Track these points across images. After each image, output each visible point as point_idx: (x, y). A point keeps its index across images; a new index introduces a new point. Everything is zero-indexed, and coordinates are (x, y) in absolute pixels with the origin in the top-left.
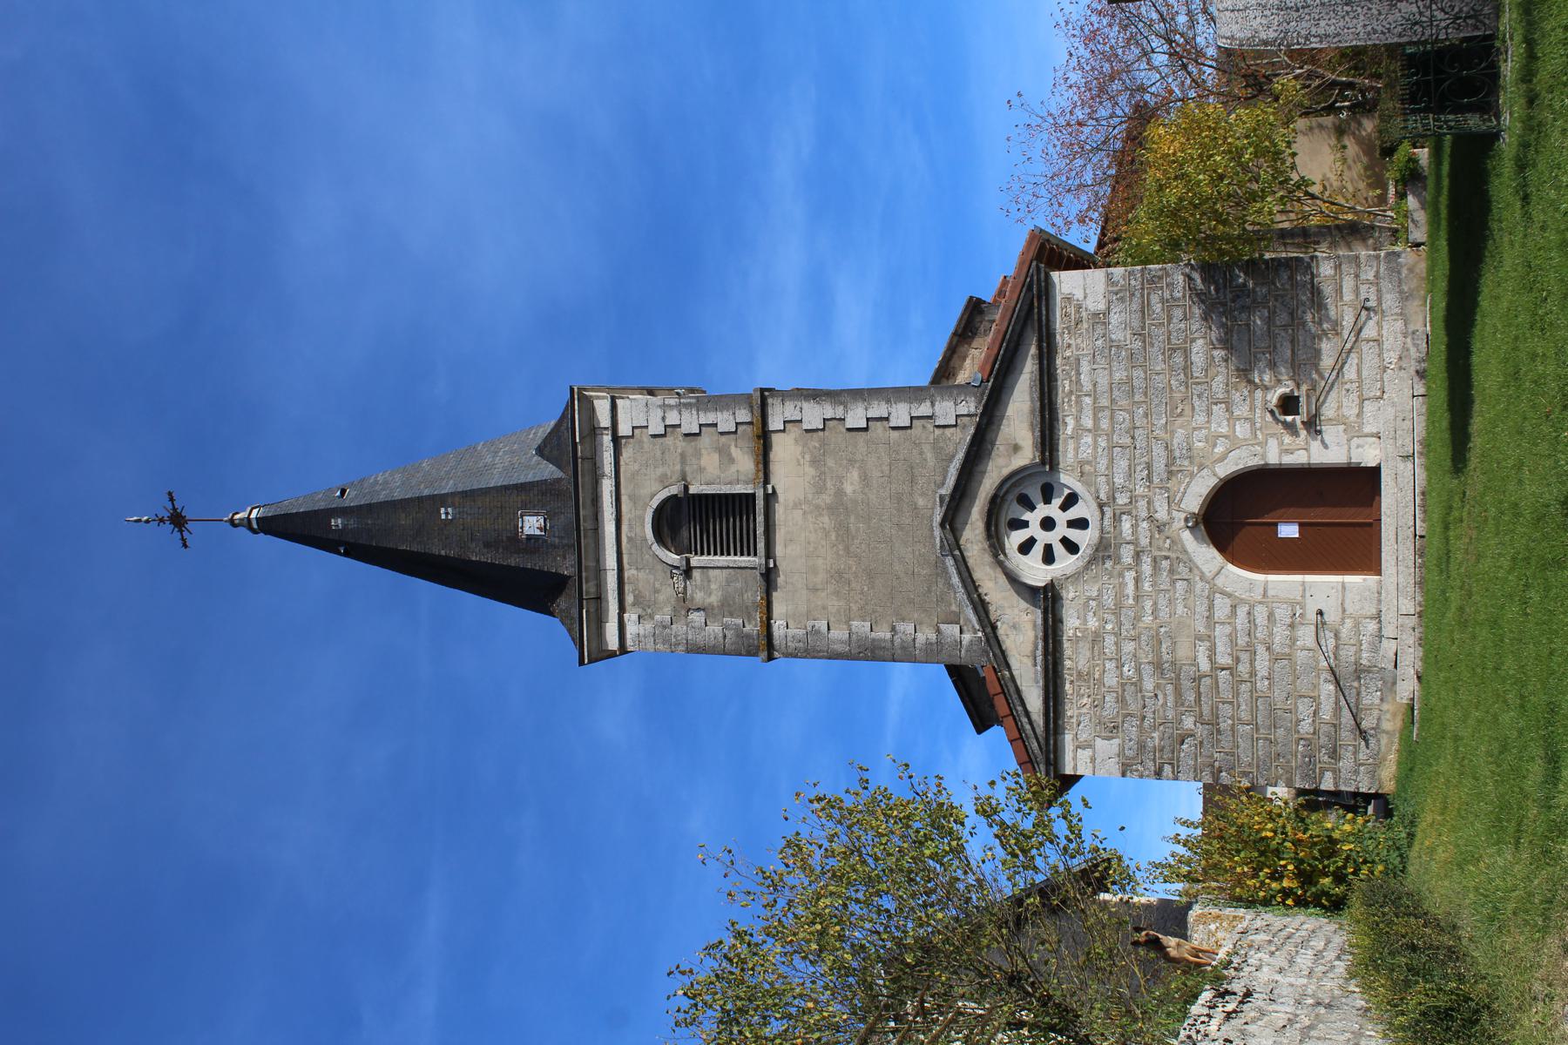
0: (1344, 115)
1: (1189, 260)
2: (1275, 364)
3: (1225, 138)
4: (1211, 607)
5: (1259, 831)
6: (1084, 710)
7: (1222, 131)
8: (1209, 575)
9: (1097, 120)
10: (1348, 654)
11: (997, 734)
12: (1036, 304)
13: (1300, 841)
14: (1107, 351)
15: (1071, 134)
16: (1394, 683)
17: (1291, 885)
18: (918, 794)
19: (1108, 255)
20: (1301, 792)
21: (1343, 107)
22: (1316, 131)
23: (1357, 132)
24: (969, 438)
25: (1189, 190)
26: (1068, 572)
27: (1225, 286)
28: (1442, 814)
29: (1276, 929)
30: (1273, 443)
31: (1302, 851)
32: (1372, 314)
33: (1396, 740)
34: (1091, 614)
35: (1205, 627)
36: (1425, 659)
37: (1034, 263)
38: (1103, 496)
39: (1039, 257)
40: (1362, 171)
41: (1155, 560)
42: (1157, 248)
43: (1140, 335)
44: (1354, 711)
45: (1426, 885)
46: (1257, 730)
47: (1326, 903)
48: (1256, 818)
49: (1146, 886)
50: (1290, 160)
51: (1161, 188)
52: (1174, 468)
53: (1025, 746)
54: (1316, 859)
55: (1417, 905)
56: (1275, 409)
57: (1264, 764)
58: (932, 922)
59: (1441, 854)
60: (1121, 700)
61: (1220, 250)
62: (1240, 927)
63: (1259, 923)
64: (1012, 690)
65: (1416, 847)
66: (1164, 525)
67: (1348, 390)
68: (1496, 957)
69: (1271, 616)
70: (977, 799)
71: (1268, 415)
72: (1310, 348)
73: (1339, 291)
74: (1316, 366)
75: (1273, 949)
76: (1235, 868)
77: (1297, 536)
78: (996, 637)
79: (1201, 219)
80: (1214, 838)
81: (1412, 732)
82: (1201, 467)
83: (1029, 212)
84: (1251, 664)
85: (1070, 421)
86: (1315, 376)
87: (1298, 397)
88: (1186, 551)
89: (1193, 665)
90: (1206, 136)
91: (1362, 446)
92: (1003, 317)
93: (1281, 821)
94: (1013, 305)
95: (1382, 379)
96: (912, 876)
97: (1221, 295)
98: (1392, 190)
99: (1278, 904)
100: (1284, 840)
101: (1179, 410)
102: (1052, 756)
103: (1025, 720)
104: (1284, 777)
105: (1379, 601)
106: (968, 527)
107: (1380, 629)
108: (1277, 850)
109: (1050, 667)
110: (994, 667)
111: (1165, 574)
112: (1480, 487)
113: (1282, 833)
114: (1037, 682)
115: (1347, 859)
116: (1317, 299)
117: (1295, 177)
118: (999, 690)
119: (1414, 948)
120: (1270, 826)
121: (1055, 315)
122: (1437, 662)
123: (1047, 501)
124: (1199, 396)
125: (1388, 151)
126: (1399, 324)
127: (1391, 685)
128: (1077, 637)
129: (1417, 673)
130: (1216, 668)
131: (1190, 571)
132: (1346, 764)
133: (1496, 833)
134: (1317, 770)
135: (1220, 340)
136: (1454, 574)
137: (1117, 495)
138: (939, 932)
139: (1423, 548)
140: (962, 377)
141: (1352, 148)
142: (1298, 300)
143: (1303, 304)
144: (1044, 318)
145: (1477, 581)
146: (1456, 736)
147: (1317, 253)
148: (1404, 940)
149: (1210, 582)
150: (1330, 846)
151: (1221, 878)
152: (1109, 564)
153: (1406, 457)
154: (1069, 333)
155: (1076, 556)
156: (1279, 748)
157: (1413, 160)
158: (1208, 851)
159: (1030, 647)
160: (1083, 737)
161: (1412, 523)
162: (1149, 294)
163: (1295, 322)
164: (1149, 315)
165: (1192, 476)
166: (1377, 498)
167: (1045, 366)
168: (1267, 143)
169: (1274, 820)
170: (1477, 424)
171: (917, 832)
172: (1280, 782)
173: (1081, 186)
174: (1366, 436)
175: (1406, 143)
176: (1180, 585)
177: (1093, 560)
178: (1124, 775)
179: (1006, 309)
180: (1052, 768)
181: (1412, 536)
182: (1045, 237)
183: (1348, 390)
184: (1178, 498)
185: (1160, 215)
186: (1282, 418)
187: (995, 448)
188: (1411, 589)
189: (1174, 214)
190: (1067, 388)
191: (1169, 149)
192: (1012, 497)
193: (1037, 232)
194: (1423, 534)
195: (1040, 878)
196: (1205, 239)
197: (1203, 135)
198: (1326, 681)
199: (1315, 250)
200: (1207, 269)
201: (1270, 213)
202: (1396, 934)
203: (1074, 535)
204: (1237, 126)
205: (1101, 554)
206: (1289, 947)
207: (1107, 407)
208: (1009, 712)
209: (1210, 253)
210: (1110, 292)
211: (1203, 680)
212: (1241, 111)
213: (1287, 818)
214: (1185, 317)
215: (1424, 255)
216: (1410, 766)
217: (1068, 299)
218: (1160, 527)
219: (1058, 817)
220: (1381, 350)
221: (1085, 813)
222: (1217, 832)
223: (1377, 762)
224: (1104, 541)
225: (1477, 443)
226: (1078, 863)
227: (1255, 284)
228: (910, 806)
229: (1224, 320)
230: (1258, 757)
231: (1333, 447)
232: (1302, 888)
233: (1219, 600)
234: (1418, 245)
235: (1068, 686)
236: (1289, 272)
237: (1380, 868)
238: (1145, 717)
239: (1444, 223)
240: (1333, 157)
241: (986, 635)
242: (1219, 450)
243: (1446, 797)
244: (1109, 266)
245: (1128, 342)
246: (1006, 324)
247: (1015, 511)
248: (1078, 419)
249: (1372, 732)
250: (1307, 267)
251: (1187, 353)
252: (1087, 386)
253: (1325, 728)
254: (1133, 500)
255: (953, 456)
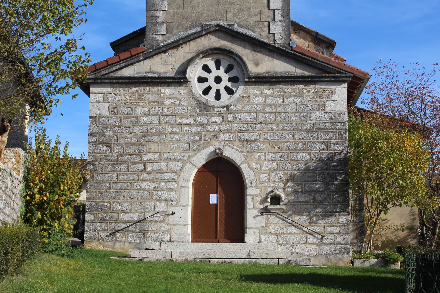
0: (419, 231)
1: (350, 153)
3: (411, 172)
4: (175, 161)
5: (63, 183)
6: (123, 97)
7: (414, 170)
8: (192, 160)
9: (424, 109)
10: (153, 227)
11: (110, 53)
12: (331, 75)
13: (59, 203)
14: (305, 111)
16: (138, 248)
17: (36, 199)
18: (77, 9)
19: (354, 112)
20: (84, 206)
21: (423, 230)
22: (412, 217)
23: (410, 237)
24: (263, 40)
25: (385, 153)
26: (193, 90)
27: (336, 170)
29: (14, 191)
30: (257, 192)
31: (54, 204)
32: (319, 240)
33: (110, 250)
34: (172, 101)
36: (150, 262)
37: (352, 75)
38: (232, 108)
40: (391, 238)
41: (199, 133)
42: (357, 137)
43: (313, 127)
44: (124, 230)
46: (114, 183)
47: (28, 215)
48: (70, 182)
49: (33, 127)
50: (398, 204)
51: (387, 139)
52: (245, 143)
53: (104, 67)
55: (29, 257)
56: (274, 193)
57: (98, 187)
58: (9, 16)
59: (53, 268)
60: (128, 116)
61: (355, 168)
62: (14, 173)
63: (16, 182)
64: (133, 61)
65: (57, 258)
66: (217, 138)
67: (282, 228)
69: (171, 190)
70: (75, 40)
71: (271, 190)
72: (304, 210)
73: (332, 225)
74: (294, 213)
75: (3, 189)
76: (44, 171)
77: (211, 203)
78: (160, 53)
79: (371, 159)
80: (59, 161)
81: (114, 256)
82: (246, 157)
83: (379, 73)
85: (270, 92)
86: (290, 213)
87: (280, 204)
89: (147, 152)
90: (412, 163)
91: (254, 234)
92: (324, 58)
93: (68, 193)
94: (330, 64)
97: (332, 168)
98: (380, 252)
99: (26, 192)
100: (59, 195)
101: (274, 146)
102: (99, 81)
103: (117, 67)
104: (91, 196)
105: (179, 242)
106: (217, 39)
107: (165, 242)
108: (54, 192)
109: (145, 80)
110: (144, 51)
111: (193, 138)
112: (233, 286)
113: (62, 194)
114: (137, 74)
115: (51, 226)
117: (389, 206)
118: (133, 54)
120: (66, 188)
121: (325, 85)
122: (149, 267)
123: (230, 80)
124: (281, 156)
125: (400, 250)
126: (314, 253)
128: (161, 94)
129: (143, 259)
131: (194, 151)
132: (98, 225)
134: (95, 212)
135: (309, 167)
137: (232, 115)
140: (294, 37)
141: (402, 234)
142: (327, 205)
143: (325, 208)
144: (323, 79)
145: (187, 284)
146: (112, 275)
147: (350, 215)
148: (10, 249)
150: (56, 217)
151: (38, 164)
152: (197, 110)
153: (249, 254)
154: (315, 92)
156: (105, 194)
157: (395, 262)
158: (53, 158)
159: (155, 70)
160: (110, 97)
161: (216, 257)
162: (333, 132)
163: (317, 204)
164: (323, 132)
165: (242, 152)
167: (298, 80)
168: (407, 192)
169: (69, 190)
170: (263, 285)
171: (57, 9)
172: (88, 194)
174: (260, 237)
176: (187, 146)
178: (90, 117)
179: (329, 60)
180: (93, 81)
181: (210, 257)
182: (365, 81)
183: (282, 228)
184: (230, 145)
185: (373, 139)
186: (269, 196)
187: (257, 53)
188: (184, 256)
189: (374, 146)
190: (287, 90)
191: (407, 144)
192: (232, 62)
193: (368, 77)
194: (211, 262)
195: (34, 73)
196: (360, 161)
197: (413, 161)
199: (352, 214)
200: (345, 162)
201: (372, 193)
202: (13, 246)
203: (212, 93)
204: (417, 178)
205: (202, 106)
207: (277, 110)
208: (121, 59)
210: (335, 113)
211: (139, 157)
212: (424, 180)
213: (70, 197)
214: (321, 150)
215: (348, 265)
217: (333, 92)
219: (67, 82)
221: (69, 96)
222: (62, 163)
223: (100, 241)
224: (209, 108)
225: (255, 285)
226: (43, 92)
228: (70, 5)
229: (319, 169)
230: (101, 183)
231: (255, 220)
232: (36, 204)
233: (179, 164)
234: (353, 263)
235: (135, 89)
236: (342, 201)
237: (47, 241)
238: (120, 128)
239: (362, 274)
240: (398, 225)
241: (161, 47)
242: (254, 166)
244: (349, 113)
245: (309, 121)
246: (321, 60)
248: (271, 96)
249: (114, 238)
250: (344, 209)
251: (303, 150)
252: (288, 101)
253: (116, 215)
254: (230, 122)
255: (253, 32)
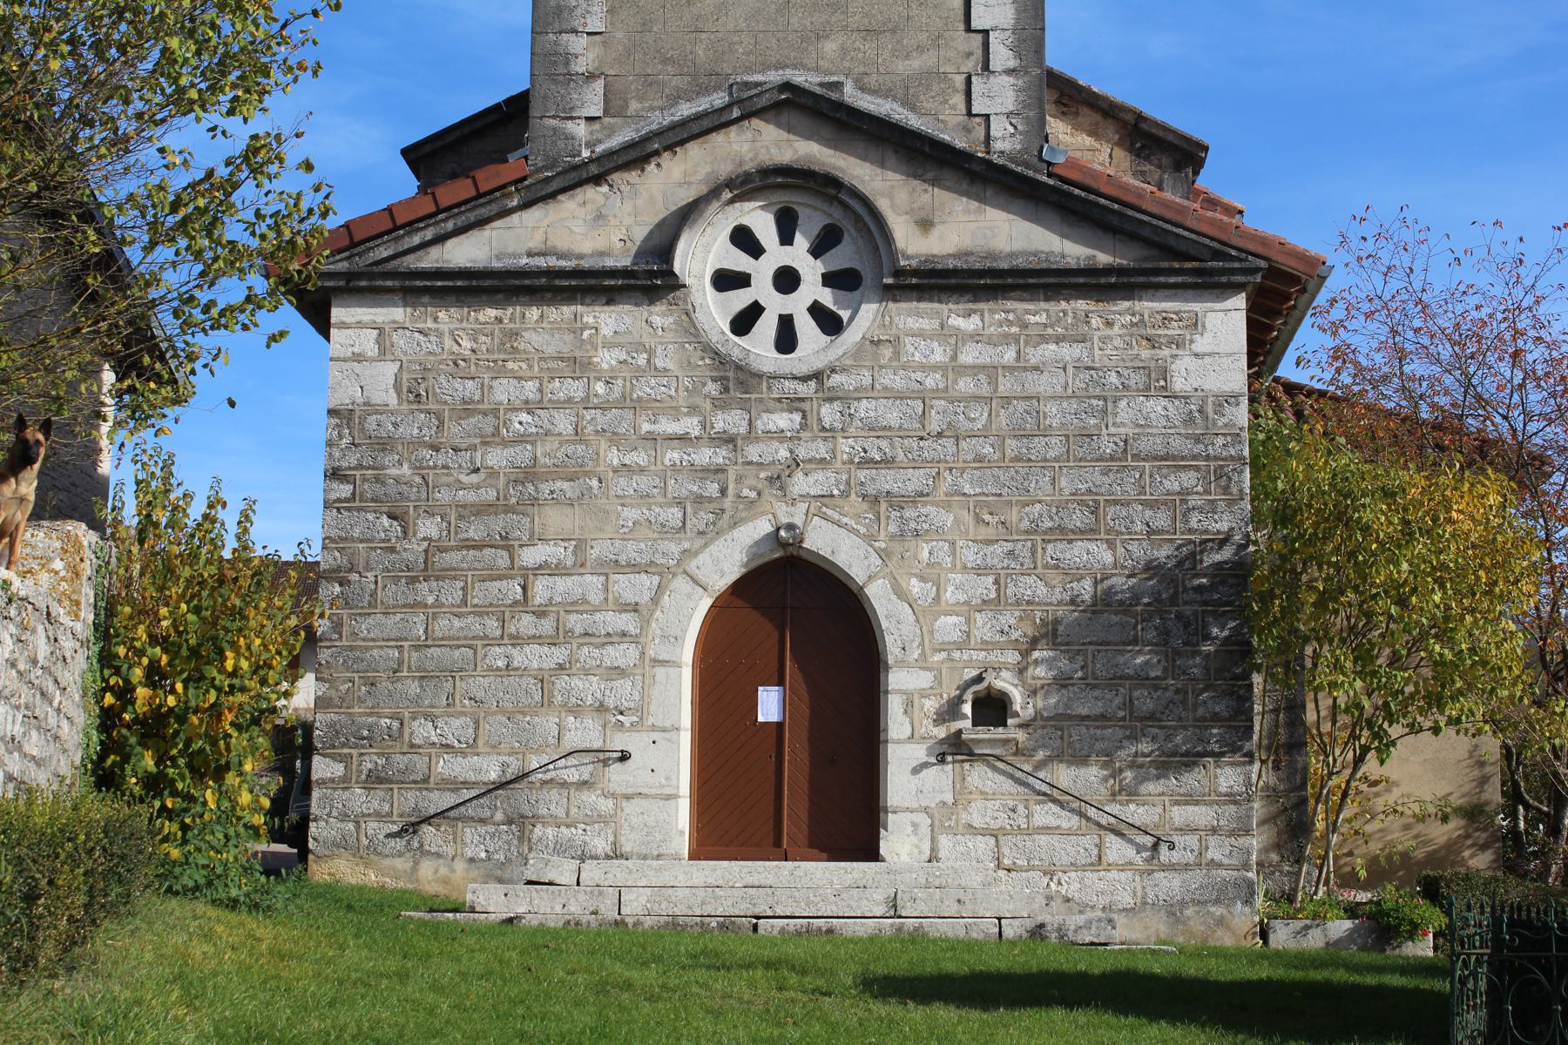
0: (1501, 821)
1: (1256, 543)
2: (1065, 686)
3: (1473, 611)
4: (634, 568)
5: (234, 645)
6: (448, 342)
8: (692, 566)
9: (1522, 386)
10: (553, 804)
11: (403, 184)
12: (1188, 265)
14: (1098, 391)
15: (1499, 337)
16: (501, 881)
17: (139, 703)
18: (284, 27)
19: (1272, 398)
20: (308, 728)
21: (1515, 819)
22: (1476, 773)
23: (1469, 842)
24: (947, 137)
25: (1381, 544)
26: (699, 316)
27: (1205, 603)
28: (271, 953)
29: (59, 675)
30: (923, 680)
31: (201, 720)
33: (401, 885)
34: (623, 356)
35: (599, 558)
36: (542, 929)
37: (1263, 264)
38: (836, 379)
39: (1274, 272)
40: (1400, 847)
41: (720, 470)
42: (1280, 486)
43: (1125, 451)
44: (452, 814)
45: (144, 925)
46: (417, 648)
47: (109, 762)
48: (258, 642)
51: (1388, 494)
52: (883, 506)
54: (188, 744)
55: (111, 910)
56: (984, 684)
58: (42, 52)
59: (198, 949)
60: (467, 409)
61: (1272, 596)
62: (59, 611)
63: (68, 644)
64: (484, 212)
65: (213, 912)
66: (781, 488)
68: (20, 1028)
69: (619, 672)
70: (278, 137)
71: (975, 673)
72: (1091, 747)
73: (1190, 800)
74: (1057, 757)
75: (21, 666)
76: (167, 605)
77: (761, 719)
78: (580, 184)
79: (1330, 564)
81: (416, 908)
82: (884, 555)
83: (1360, 259)
84: (534, 637)
85: (970, 324)
86: (1040, 755)
87: (1005, 725)
88: (734, 524)
90: (1478, 578)
91: (915, 832)
93: (252, 684)
94: (1188, 223)
95: (1033, 868)
96: (128, 15)
97: (1192, 596)
98: (1363, 897)
100: (219, 690)
101: (987, 517)
102: (364, 283)
103: (429, 234)
104: (333, 693)
106: (784, 135)
107: (596, 858)
108: (202, 678)
109: (527, 282)
110: (525, 178)
111: (695, 488)
112: (836, 1016)
113: (232, 687)
114: (498, 258)
115: (190, 798)
116: (1176, 761)
117: (1395, 731)
118: (483, 188)
119: (31, 898)
120: (245, 664)
122: (537, 948)
123: (829, 280)
124: (1011, 553)
125: (1432, 891)
126: (1127, 900)
127: (498, 874)
128: (582, 330)
129: (518, 918)
130: (527, 577)
131: (701, 533)
132: (358, 799)
133: (237, 1032)
134: (346, 751)
135: (1109, 592)
136: (690, 976)
137: (837, 405)
138: (24, 65)
139: (736, 929)
140: (1058, 129)
141: (1440, 833)
142: (1175, 728)
143: (1168, 738)
144: (1162, 279)
145: (676, 1009)
146: (408, 977)
148: (44, 882)
149: (680, 567)
150: (211, 768)
151: (146, 580)
152: (712, 388)
154: (1133, 325)
155: (727, 330)
156: (384, 685)
157: (1414, 931)
159: (562, 244)
160: (400, 340)
161: (779, 912)
162: (1197, 469)
163: (1137, 723)
164: (1160, 468)
165: (870, 539)
166: (825, 855)
168: (1459, 684)
169: (255, 672)
170: (945, 1014)
171: (213, 26)
172: (324, 687)
173: (1401, 356)
174: (933, 840)
175: (1445, 920)
177: (720, 359)
178: (332, 412)
179: (1182, 210)
180: (342, 283)
181: (757, 911)
182: (1311, 287)
184: (829, 512)
186: (969, 696)
187: (926, 186)
188: (665, 908)
189: (1341, 517)
190: (1032, 319)
192: (837, 215)
193: (1321, 270)
194: (761, 931)
195: (133, 254)
196: (1293, 571)
197: (1482, 573)
198: (504, 765)
199: (1263, 762)
200: (1237, 573)
201: (1333, 685)
202: (54, 871)
203: (766, 327)
204: (1494, 632)
205: (731, 374)
206: (26, 694)
207: (996, 390)
209: (1267, 579)
210: (1204, 400)
211: (505, 554)
212: (1520, 641)
213: (259, 695)
214: (1154, 532)
215: (1248, 943)
216: (357, 905)
217: (1195, 324)
218: (778, 481)
219: (250, 288)
220: (1084, 868)
221: (257, 338)
222: (231, 574)
223: (364, 853)
224: (754, 381)
225: (916, 1014)
226: (165, 323)
227: (1208, 655)
228: (261, 12)
229: (1146, 600)
230: (368, 648)
231: (916, 781)
232: (136, 720)
233: (647, 582)
234: (1264, 935)
235: (492, 313)
237: (175, 853)
238: (437, 451)
239: (1298, 975)
241: (585, 164)
242: (915, 587)
243: (300, 958)
244: (1252, 400)
245: (1112, 430)
246: (1155, 210)
247: (811, 222)
248: (976, 337)
249: (416, 844)
250: (1235, 744)
251: (1089, 533)
252: (1034, 355)
253: (420, 763)
254: (827, 432)
255: (913, 108)
